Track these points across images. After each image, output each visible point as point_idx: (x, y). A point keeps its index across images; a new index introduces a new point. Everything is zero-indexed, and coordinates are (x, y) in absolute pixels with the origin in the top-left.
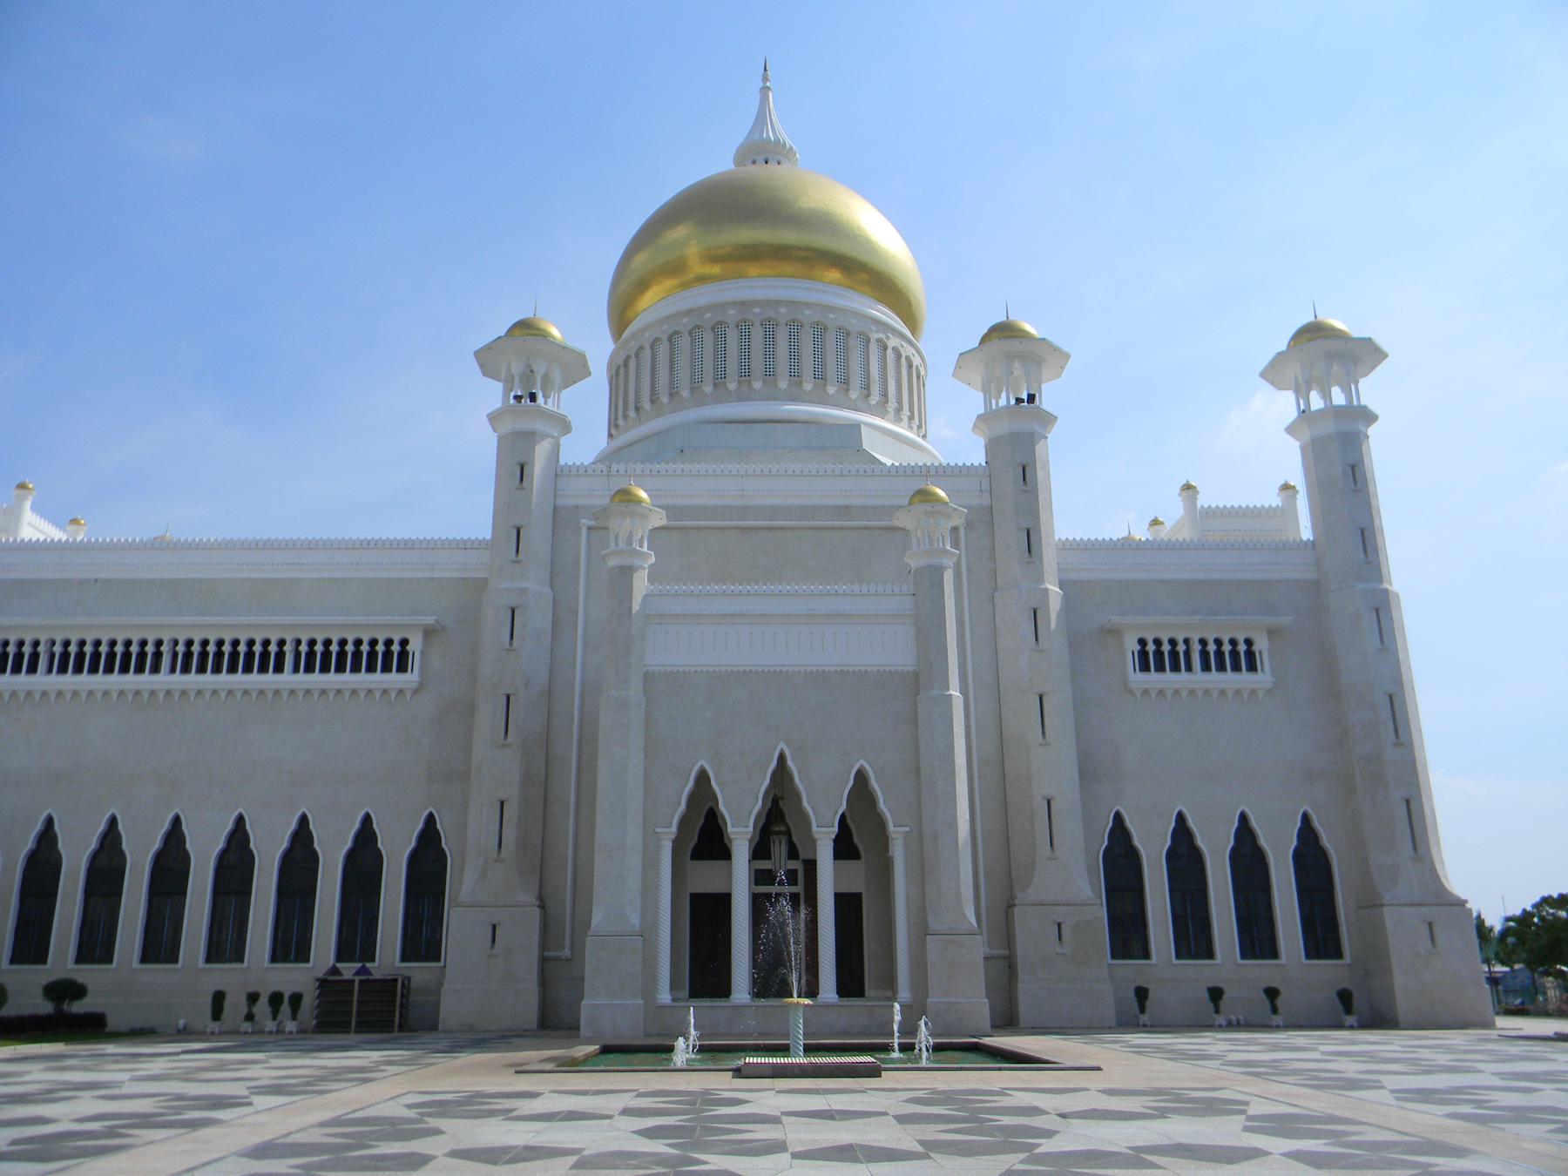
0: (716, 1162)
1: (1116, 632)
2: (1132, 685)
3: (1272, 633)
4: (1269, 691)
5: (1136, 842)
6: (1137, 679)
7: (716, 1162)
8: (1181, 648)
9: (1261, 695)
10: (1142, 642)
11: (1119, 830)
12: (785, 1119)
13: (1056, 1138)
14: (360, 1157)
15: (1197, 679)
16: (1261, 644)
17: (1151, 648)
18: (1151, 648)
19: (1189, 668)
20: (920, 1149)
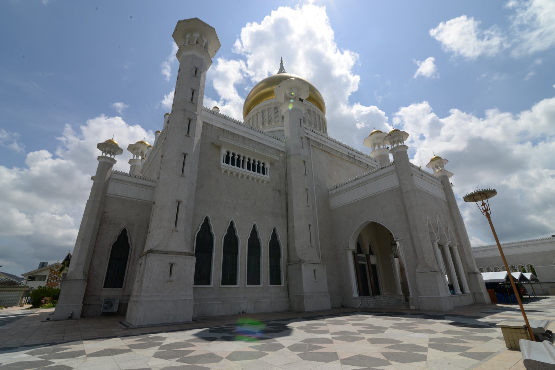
0: (57, 362)
1: (219, 147)
2: (222, 167)
3: (271, 164)
4: (268, 182)
5: (213, 231)
6: (223, 164)
7: (57, 362)
8: (242, 159)
9: (265, 183)
10: (228, 153)
11: (206, 225)
12: (334, 341)
13: (153, 354)
14: (67, 353)
15: (244, 171)
16: (267, 166)
17: (231, 155)
18: (231, 155)
19: (243, 167)
20: (357, 332)
